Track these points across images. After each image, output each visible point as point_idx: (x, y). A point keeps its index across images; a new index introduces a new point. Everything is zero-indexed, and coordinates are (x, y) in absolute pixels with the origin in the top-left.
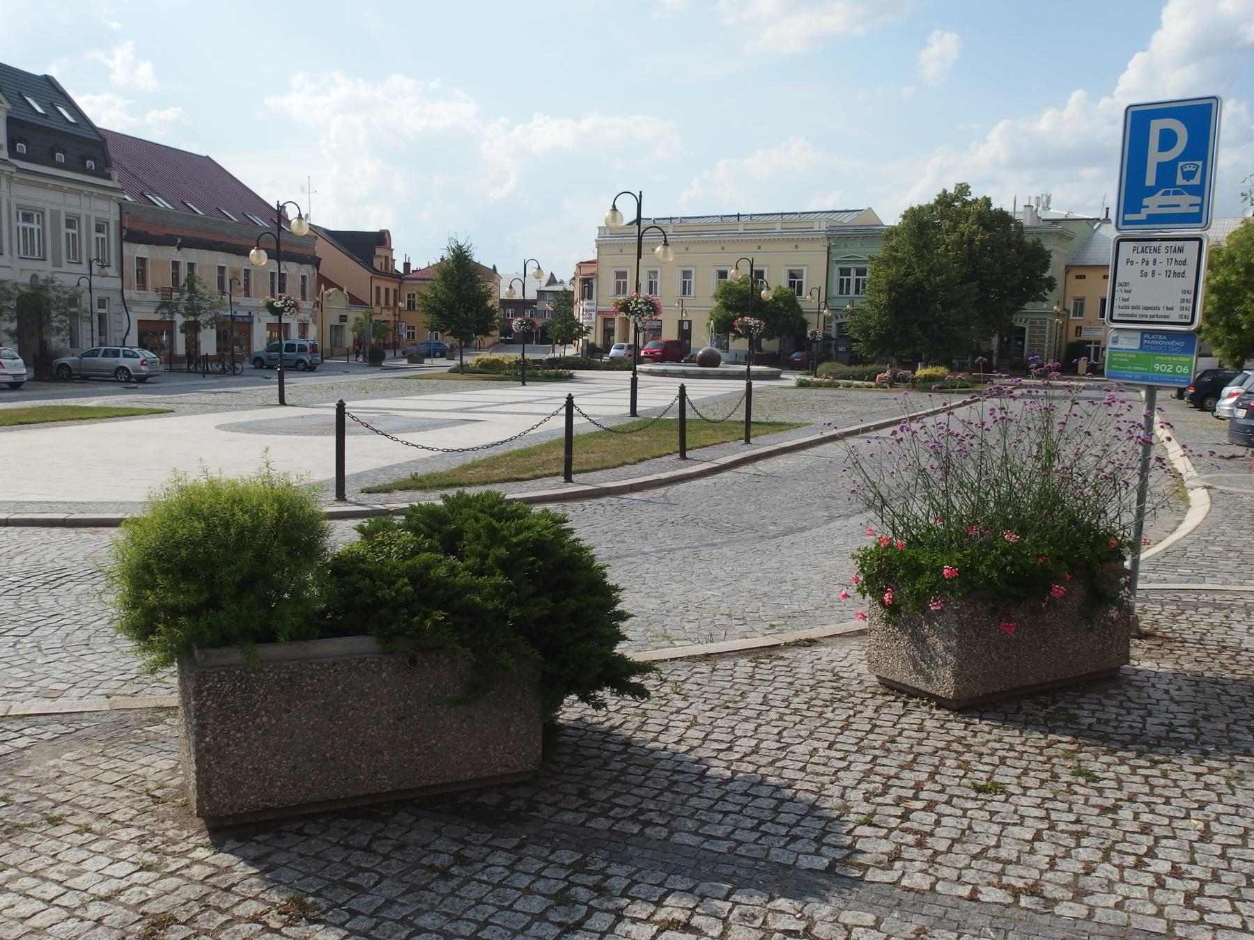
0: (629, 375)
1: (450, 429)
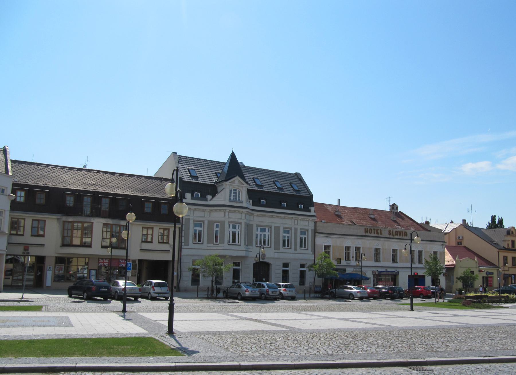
0: (166, 304)
1: (210, 330)
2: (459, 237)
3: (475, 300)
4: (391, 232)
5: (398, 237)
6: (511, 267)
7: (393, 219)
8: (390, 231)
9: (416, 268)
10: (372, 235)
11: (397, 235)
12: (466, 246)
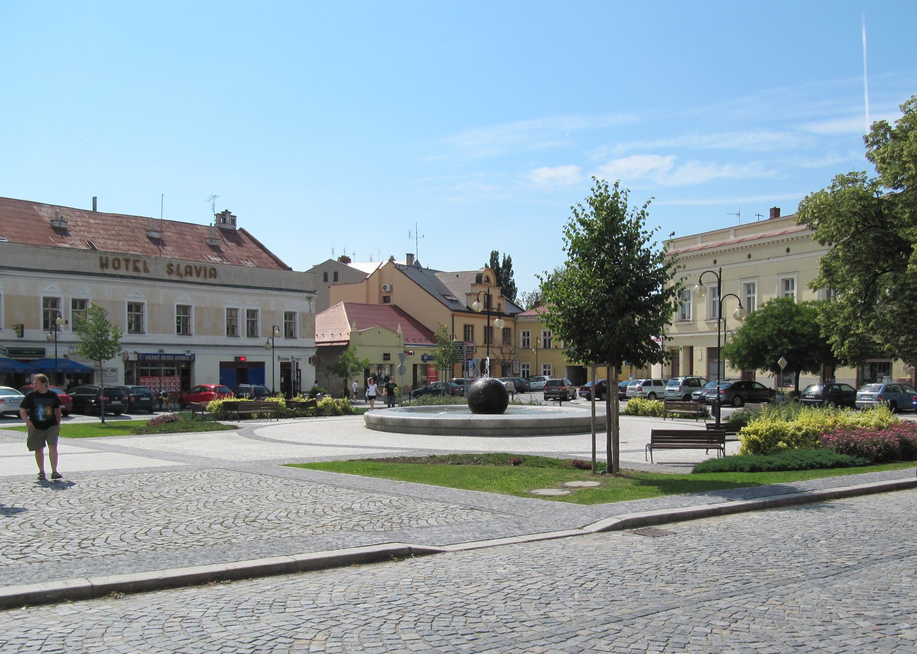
2: (385, 287)
3: (696, 412)
4: (174, 268)
5: (194, 278)
6: (482, 345)
7: (211, 241)
8: (171, 265)
9: (241, 346)
10: (122, 272)
11: (191, 274)
12: (398, 305)
